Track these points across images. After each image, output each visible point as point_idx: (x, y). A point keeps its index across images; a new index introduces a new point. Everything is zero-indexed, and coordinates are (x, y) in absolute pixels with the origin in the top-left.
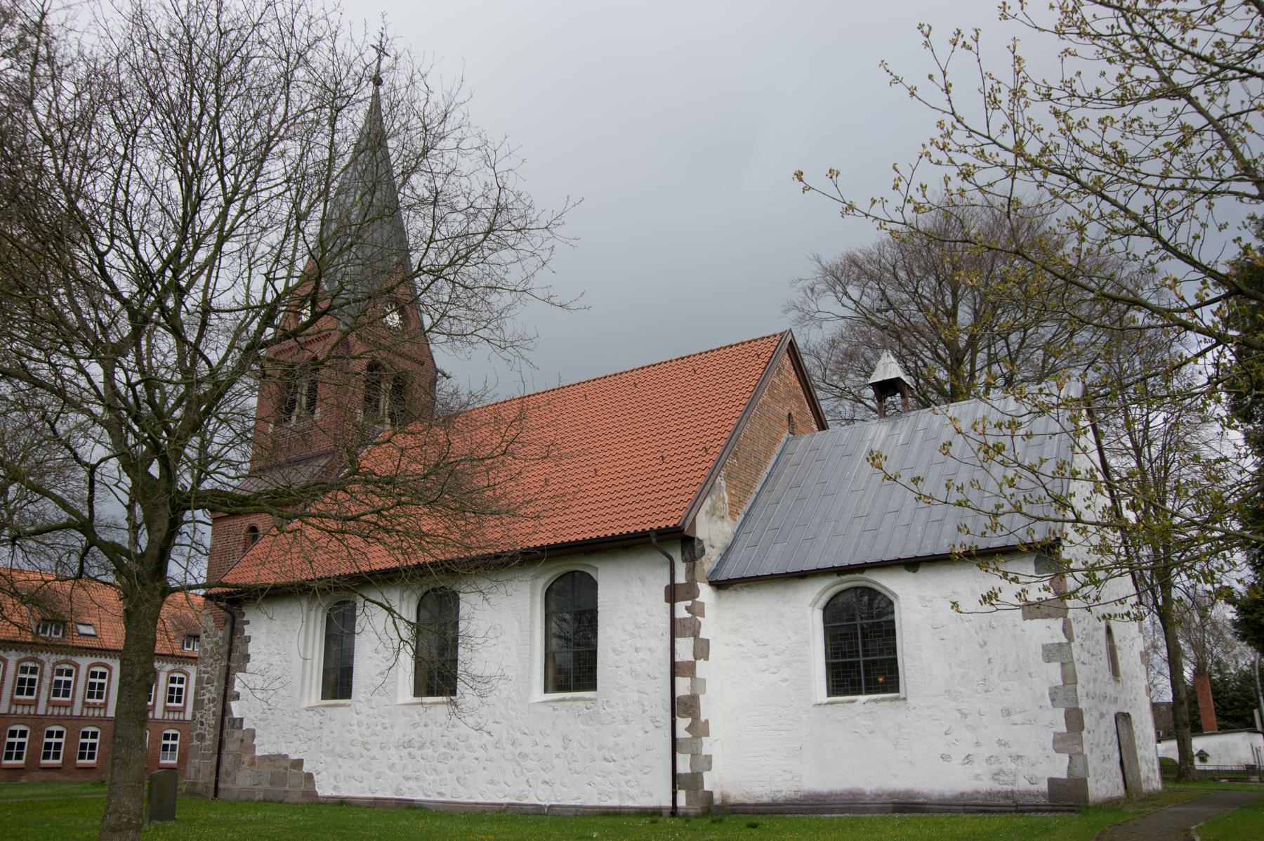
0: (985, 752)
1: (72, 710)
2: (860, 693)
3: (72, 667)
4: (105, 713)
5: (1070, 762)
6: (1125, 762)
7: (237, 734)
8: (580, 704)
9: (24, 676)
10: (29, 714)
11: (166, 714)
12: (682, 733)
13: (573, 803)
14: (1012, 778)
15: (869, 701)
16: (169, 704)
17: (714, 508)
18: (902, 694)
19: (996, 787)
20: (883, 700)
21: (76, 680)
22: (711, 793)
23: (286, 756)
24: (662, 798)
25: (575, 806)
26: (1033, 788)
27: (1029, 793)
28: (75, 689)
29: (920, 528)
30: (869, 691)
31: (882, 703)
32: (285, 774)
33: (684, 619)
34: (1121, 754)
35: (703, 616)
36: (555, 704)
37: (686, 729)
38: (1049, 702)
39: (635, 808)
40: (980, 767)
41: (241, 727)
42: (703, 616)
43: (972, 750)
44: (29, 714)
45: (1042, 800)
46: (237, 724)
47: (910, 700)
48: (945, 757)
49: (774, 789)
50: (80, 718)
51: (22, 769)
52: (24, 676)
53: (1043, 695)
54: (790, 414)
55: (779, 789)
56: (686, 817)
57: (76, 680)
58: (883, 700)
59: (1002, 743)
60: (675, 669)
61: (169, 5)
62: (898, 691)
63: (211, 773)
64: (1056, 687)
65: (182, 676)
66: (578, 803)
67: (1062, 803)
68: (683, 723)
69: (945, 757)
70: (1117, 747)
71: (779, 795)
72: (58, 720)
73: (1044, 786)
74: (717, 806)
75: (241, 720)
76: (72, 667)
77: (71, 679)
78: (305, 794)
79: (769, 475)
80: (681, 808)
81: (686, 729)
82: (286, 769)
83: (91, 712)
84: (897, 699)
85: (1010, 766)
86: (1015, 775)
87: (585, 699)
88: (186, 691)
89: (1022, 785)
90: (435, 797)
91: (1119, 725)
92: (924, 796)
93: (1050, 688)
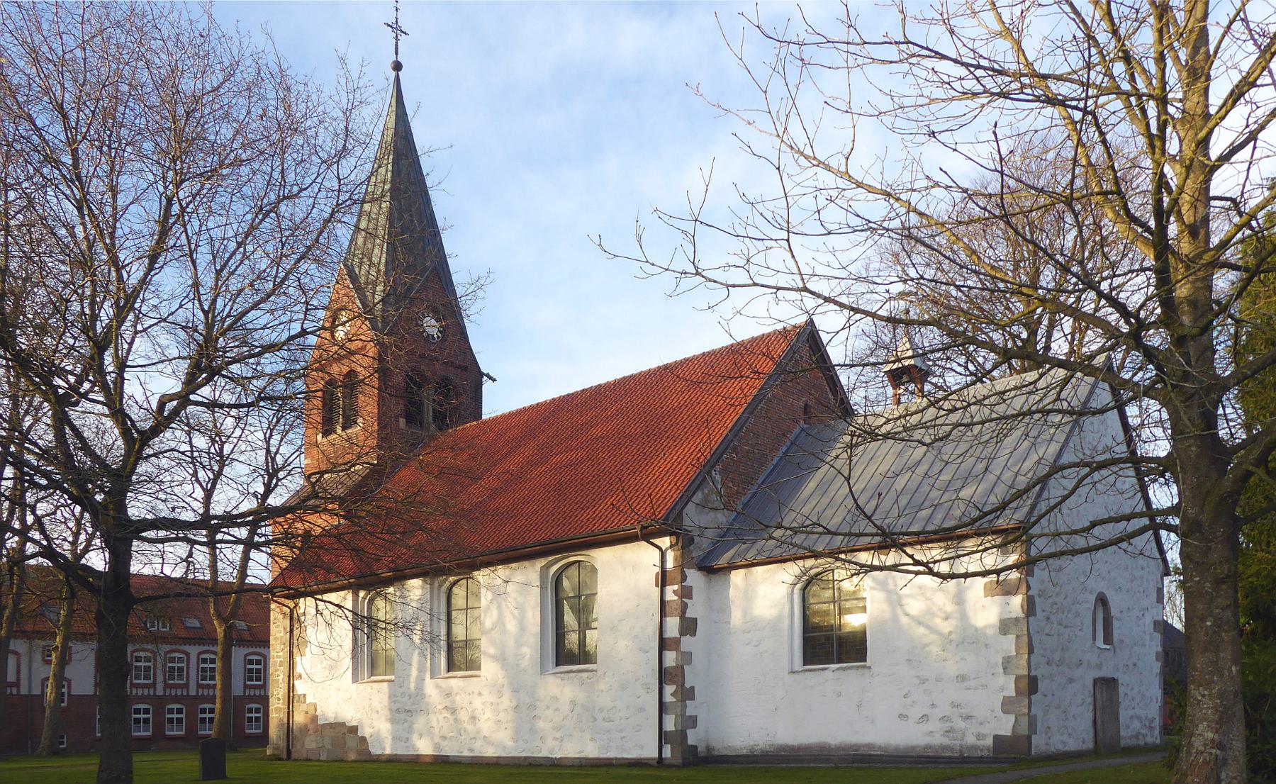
0: (938, 713)
1: (155, 691)
2: (832, 663)
3: (182, 656)
4: (188, 692)
5: (1015, 721)
6: (1099, 722)
7: (303, 707)
8: (585, 675)
9: (173, 665)
10: (149, 695)
11: (200, 691)
12: (668, 698)
13: (577, 756)
14: (961, 735)
15: (838, 669)
16: (248, 683)
17: (706, 499)
18: (868, 663)
19: (946, 741)
20: (851, 668)
21: (188, 666)
22: (696, 747)
23: (344, 723)
24: (649, 751)
25: (579, 758)
26: (980, 743)
27: (974, 748)
28: (188, 674)
29: (940, 516)
30: (840, 661)
31: (849, 671)
32: (344, 738)
33: (671, 601)
34: (1095, 713)
35: (691, 598)
36: (562, 675)
37: (671, 695)
38: (1001, 670)
39: (627, 759)
40: (935, 725)
41: (305, 702)
42: (691, 598)
43: (926, 711)
44: (149, 695)
45: (986, 753)
46: (302, 699)
47: (874, 669)
48: (903, 717)
49: (752, 743)
50: (196, 697)
51: (150, 739)
52: (173, 665)
53: (996, 664)
54: (806, 405)
55: (756, 743)
56: (671, 766)
57: (155, 666)
58: (858, 667)
59: (955, 705)
60: (663, 644)
61: (1086, 9)
62: (865, 661)
63: (472, 750)
64: (1009, 657)
65: (213, 656)
66: (582, 755)
67: (1005, 755)
68: (669, 689)
69: (903, 717)
70: (1091, 708)
71: (756, 748)
72: (176, 699)
73: (989, 742)
74: (701, 757)
75: (305, 695)
76: (182, 656)
77: (183, 665)
78: (359, 753)
79: (775, 466)
80: (666, 758)
81: (671, 695)
82: (344, 734)
83: (173, 692)
84: (864, 667)
85: (961, 724)
86: (964, 733)
87: (587, 671)
88: (188, 670)
89: (970, 740)
90: (466, 753)
91: (1097, 689)
92: (880, 748)
93: (1003, 658)
